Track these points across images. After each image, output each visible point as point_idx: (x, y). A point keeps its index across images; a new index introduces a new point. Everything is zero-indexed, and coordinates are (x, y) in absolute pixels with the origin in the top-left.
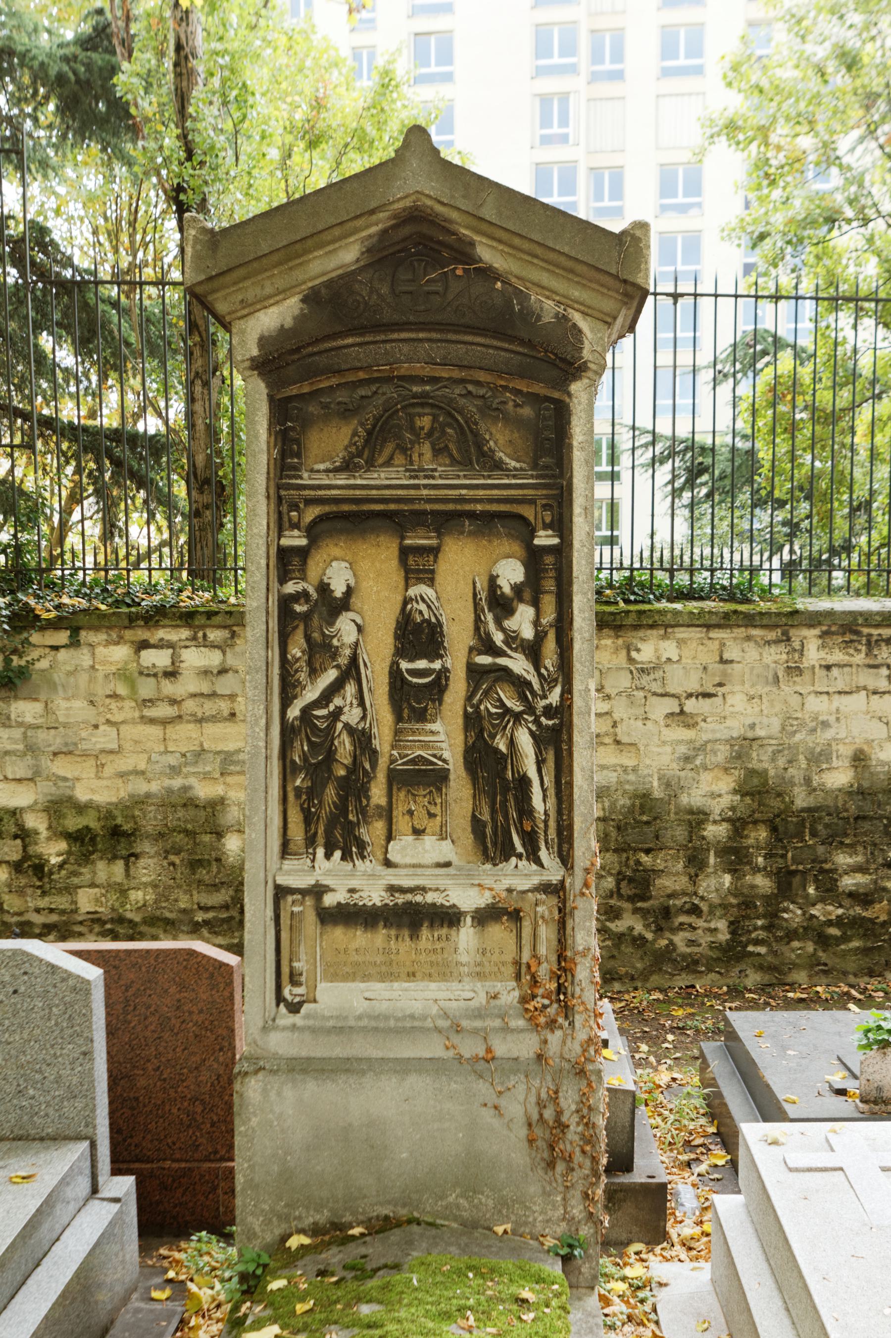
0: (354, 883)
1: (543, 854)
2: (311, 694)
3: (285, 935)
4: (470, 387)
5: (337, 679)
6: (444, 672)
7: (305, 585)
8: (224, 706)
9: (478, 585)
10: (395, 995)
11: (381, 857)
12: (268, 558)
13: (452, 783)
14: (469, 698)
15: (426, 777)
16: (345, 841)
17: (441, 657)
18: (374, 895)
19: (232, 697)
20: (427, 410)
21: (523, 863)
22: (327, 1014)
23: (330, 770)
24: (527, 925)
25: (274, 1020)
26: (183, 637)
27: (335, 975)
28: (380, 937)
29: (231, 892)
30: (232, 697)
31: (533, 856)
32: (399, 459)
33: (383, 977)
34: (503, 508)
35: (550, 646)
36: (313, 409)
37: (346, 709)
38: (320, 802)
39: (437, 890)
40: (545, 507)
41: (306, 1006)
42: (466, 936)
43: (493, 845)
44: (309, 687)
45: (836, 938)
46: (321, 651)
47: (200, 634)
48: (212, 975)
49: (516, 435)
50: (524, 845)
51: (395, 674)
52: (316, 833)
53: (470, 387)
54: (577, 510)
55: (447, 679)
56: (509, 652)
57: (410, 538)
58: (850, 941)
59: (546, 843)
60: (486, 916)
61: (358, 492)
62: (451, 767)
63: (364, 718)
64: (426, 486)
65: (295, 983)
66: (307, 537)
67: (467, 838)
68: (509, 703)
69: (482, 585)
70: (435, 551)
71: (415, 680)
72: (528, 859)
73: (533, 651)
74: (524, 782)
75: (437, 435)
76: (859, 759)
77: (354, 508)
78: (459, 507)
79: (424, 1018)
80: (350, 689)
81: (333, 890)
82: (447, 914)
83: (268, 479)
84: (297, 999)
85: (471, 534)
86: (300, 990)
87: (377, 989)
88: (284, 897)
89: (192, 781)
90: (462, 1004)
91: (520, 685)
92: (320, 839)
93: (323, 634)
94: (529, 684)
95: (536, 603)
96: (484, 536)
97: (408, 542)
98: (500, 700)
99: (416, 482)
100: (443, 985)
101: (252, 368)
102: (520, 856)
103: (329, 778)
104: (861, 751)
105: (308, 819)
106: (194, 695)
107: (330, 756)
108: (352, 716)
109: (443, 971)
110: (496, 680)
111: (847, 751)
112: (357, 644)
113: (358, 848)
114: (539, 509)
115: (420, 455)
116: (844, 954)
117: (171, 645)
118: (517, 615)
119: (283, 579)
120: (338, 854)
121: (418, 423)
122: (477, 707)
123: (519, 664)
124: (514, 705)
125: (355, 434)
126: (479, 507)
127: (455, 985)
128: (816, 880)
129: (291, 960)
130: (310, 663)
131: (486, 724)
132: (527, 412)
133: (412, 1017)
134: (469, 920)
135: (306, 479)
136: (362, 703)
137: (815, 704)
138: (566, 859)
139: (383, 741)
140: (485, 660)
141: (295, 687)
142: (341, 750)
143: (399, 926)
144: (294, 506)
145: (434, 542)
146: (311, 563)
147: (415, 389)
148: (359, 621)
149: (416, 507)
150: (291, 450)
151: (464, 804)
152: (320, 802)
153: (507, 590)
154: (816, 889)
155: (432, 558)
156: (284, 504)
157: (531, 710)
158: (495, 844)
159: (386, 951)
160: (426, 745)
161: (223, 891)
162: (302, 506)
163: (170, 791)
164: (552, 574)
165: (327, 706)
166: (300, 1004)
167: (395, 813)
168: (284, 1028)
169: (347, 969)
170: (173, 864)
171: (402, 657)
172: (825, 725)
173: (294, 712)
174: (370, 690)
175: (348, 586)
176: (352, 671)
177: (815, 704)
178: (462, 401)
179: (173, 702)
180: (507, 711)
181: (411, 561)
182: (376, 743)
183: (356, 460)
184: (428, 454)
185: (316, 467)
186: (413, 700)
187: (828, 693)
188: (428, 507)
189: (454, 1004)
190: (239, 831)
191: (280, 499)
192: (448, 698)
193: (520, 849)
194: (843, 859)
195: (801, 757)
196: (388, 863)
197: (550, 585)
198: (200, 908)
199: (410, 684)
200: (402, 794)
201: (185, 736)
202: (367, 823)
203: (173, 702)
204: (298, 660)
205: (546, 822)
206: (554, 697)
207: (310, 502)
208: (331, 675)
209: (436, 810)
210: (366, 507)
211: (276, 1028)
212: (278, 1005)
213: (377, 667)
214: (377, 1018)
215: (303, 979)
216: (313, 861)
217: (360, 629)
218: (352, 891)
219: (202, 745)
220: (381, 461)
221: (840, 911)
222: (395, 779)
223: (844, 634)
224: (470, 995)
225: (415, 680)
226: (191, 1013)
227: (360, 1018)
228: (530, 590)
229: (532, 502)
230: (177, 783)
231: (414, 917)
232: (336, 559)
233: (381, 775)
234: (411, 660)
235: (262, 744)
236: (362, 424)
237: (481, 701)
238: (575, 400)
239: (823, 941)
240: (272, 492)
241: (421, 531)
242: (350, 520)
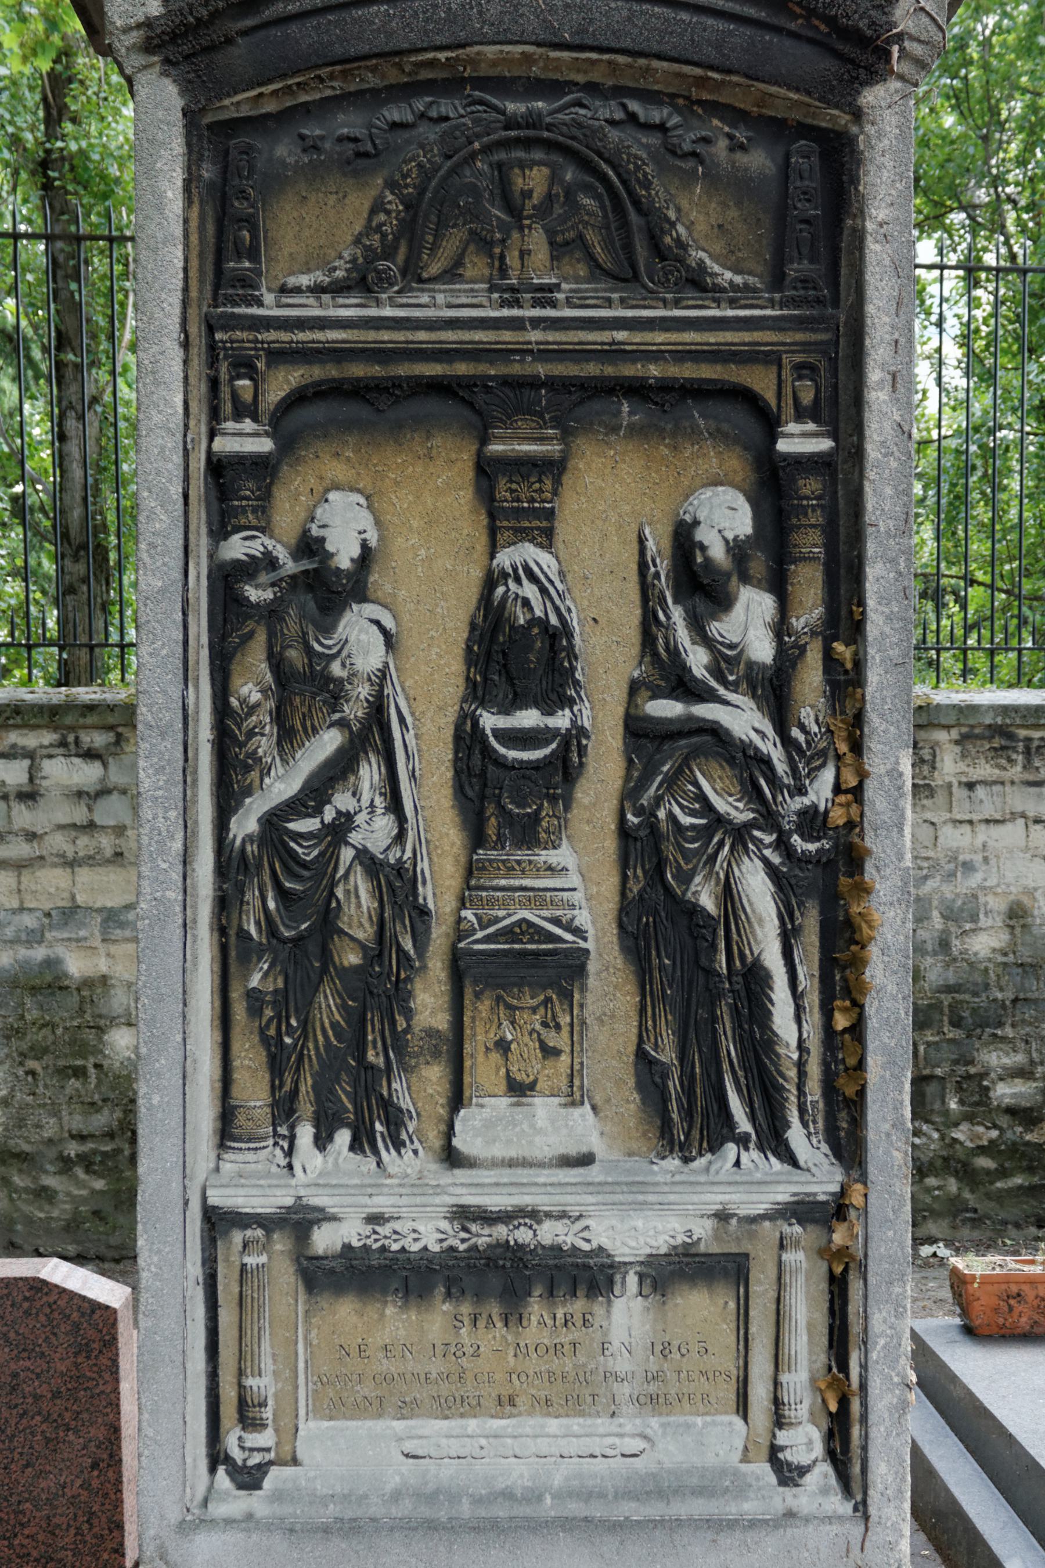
0: (381, 1203)
1: (796, 1136)
2: (282, 785)
3: (227, 1317)
4: (634, 106)
5: (340, 751)
6: (574, 741)
7: (270, 543)
8: (106, 843)
9: (650, 544)
10: (469, 1447)
11: (437, 1143)
12: (186, 479)
13: (592, 982)
14: (630, 794)
15: (538, 969)
16: (370, 1120)
17: (570, 702)
18: (426, 1231)
19: (120, 830)
20: (538, 155)
21: (752, 1157)
22: (321, 1489)
23: (326, 955)
24: (761, 1287)
25: (205, 1502)
26: (46, 742)
27: (335, 1407)
28: (437, 1319)
29: (118, 1114)
30: (120, 830)
31: (773, 1140)
32: (476, 266)
33: (449, 1407)
34: (707, 372)
35: (810, 680)
36: (285, 151)
37: (360, 819)
38: (305, 1024)
39: (563, 1215)
40: (802, 370)
41: (274, 1471)
42: (627, 1315)
43: (684, 1115)
44: (279, 769)
45: (988, 1172)
46: (306, 689)
47: (71, 738)
48: (77, 1326)
49: (733, 213)
50: (752, 1117)
51: (468, 740)
52: (295, 1092)
53: (634, 106)
54: (874, 375)
55: (582, 751)
56: (722, 691)
57: (502, 439)
58: (1012, 1175)
59: (802, 1111)
60: (672, 1272)
61: (386, 336)
62: (589, 945)
63: (400, 837)
64: (536, 323)
65: (248, 1421)
66: (273, 435)
67: (627, 1101)
68: (721, 805)
69: (659, 543)
70: (553, 469)
71: (513, 754)
72: (761, 1149)
73: (774, 689)
74: (753, 980)
75: (558, 210)
76: (1017, 915)
77: (377, 370)
78: (609, 370)
79: (534, 1496)
80: (369, 773)
81: (334, 1218)
82: (587, 1267)
83: (185, 304)
84: (256, 1459)
85: (635, 432)
86: (265, 1438)
87: (432, 1432)
88: (226, 1233)
89: (60, 951)
90: (618, 1463)
91: (746, 763)
92: (306, 1107)
93: (309, 650)
94: (766, 762)
95: (779, 586)
96: (661, 433)
97: (496, 448)
98: (702, 797)
99: (515, 312)
100: (576, 1424)
101: (148, 47)
102: (743, 1141)
103: (324, 970)
104: (1019, 904)
105: (278, 1062)
106: (61, 827)
107: (329, 922)
108: (375, 832)
109: (576, 1394)
110: (694, 753)
111: (997, 904)
112: (383, 673)
113: (388, 1124)
114: (787, 373)
115: (523, 254)
116: (1000, 1198)
117: (30, 755)
118: (739, 608)
119: (221, 529)
120: (343, 1137)
121: (519, 184)
122: (648, 814)
123: (743, 719)
124: (733, 808)
125: (378, 206)
126: (654, 371)
127: (602, 1424)
128: (959, 1088)
129: (241, 1373)
130: (279, 717)
131: (670, 851)
132: (758, 161)
133: (508, 1495)
134: (632, 1280)
135: (270, 307)
136: (395, 806)
137: (953, 838)
138: (848, 1147)
139: (439, 888)
140: (666, 709)
141: (248, 769)
142: (350, 909)
143: (479, 1297)
144: (245, 366)
145: (553, 449)
146: (281, 496)
147: (511, 107)
148: (389, 623)
149: (516, 369)
150: (237, 242)
151: (620, 1027)
152: (305, 1024)
153: (718, 552)
154: (961, 1102)
155: (548, 484)
156: (224, 357)
157: (769, 818)
158: (688, 1114)
159: (451, 1350)
160: (536, 897)
161: (106, 1112)
162: (260, 365)
163: (25, 965)
164: (816, 518)
165: (318, 811)
166: (262, 1469)
167: (468, 1048)
168: (229, 1522)
169: (367, 1389)
170: (32, 1073)
171: (482, 704)
172: (968, 867)
173: (246, 824)
174: (413, 776)
175: (364, 545)
176: (374, 733)
177: (953, 838)
178: (614, 135)
179: (31, 836)
180: (718, 821)
181: (502, 492)
182: (426, 893)
183: (382, 265)
184: (541, 253)
185: (292, 281)
186: (506, 798)
187: (970, 822)
188: (542, 370)
189: (599, 1464)
190: (130, 1024)
191: (212, 347)
192: (585, 793)
193: (744, 1125)
194: (995, 1059)
195: (935, 913)
196: (452, 1157)
197: (811, 542)
198: (72, 1137)
199: (501, 763)
200: (485, 1006)
201: (51, 884)
202: (407, 1069)
203: (31, 836)
204: (253, 709)
205: (801, 1065)
206: (821, 789)
207: (279, 356)
208: (329, 742)
209: (559, 1040)
210: (403, 370)
211: (205, 1523)
212: (212, 1470)
213: (428, 727)
214: (431, 1498)
215: (268, 1413)
216: (289, 1153)
217: (390, 640)
218: (375, 1219)
219: (73, 898)
220: (434, 269)
221: (994, 1134)
222: (460, 969)
223: (991, 738)
224: (635, 1445)
225: (513, 754)
226: (37, 1398)
227: (396, 1496)
228: (770, 555)
229: (770, 358)
230: (39, 953)
231: (508, 1274)
232: (337, 487)
233: (437, 966)
234: (506, 712)
235: (174, 895)
236: (391, 185)
237: (658, 801)
238: (869, 129)
239: (967, 1174)
240: (193, 330)
241: (525, 425)
242: (366, 399)
